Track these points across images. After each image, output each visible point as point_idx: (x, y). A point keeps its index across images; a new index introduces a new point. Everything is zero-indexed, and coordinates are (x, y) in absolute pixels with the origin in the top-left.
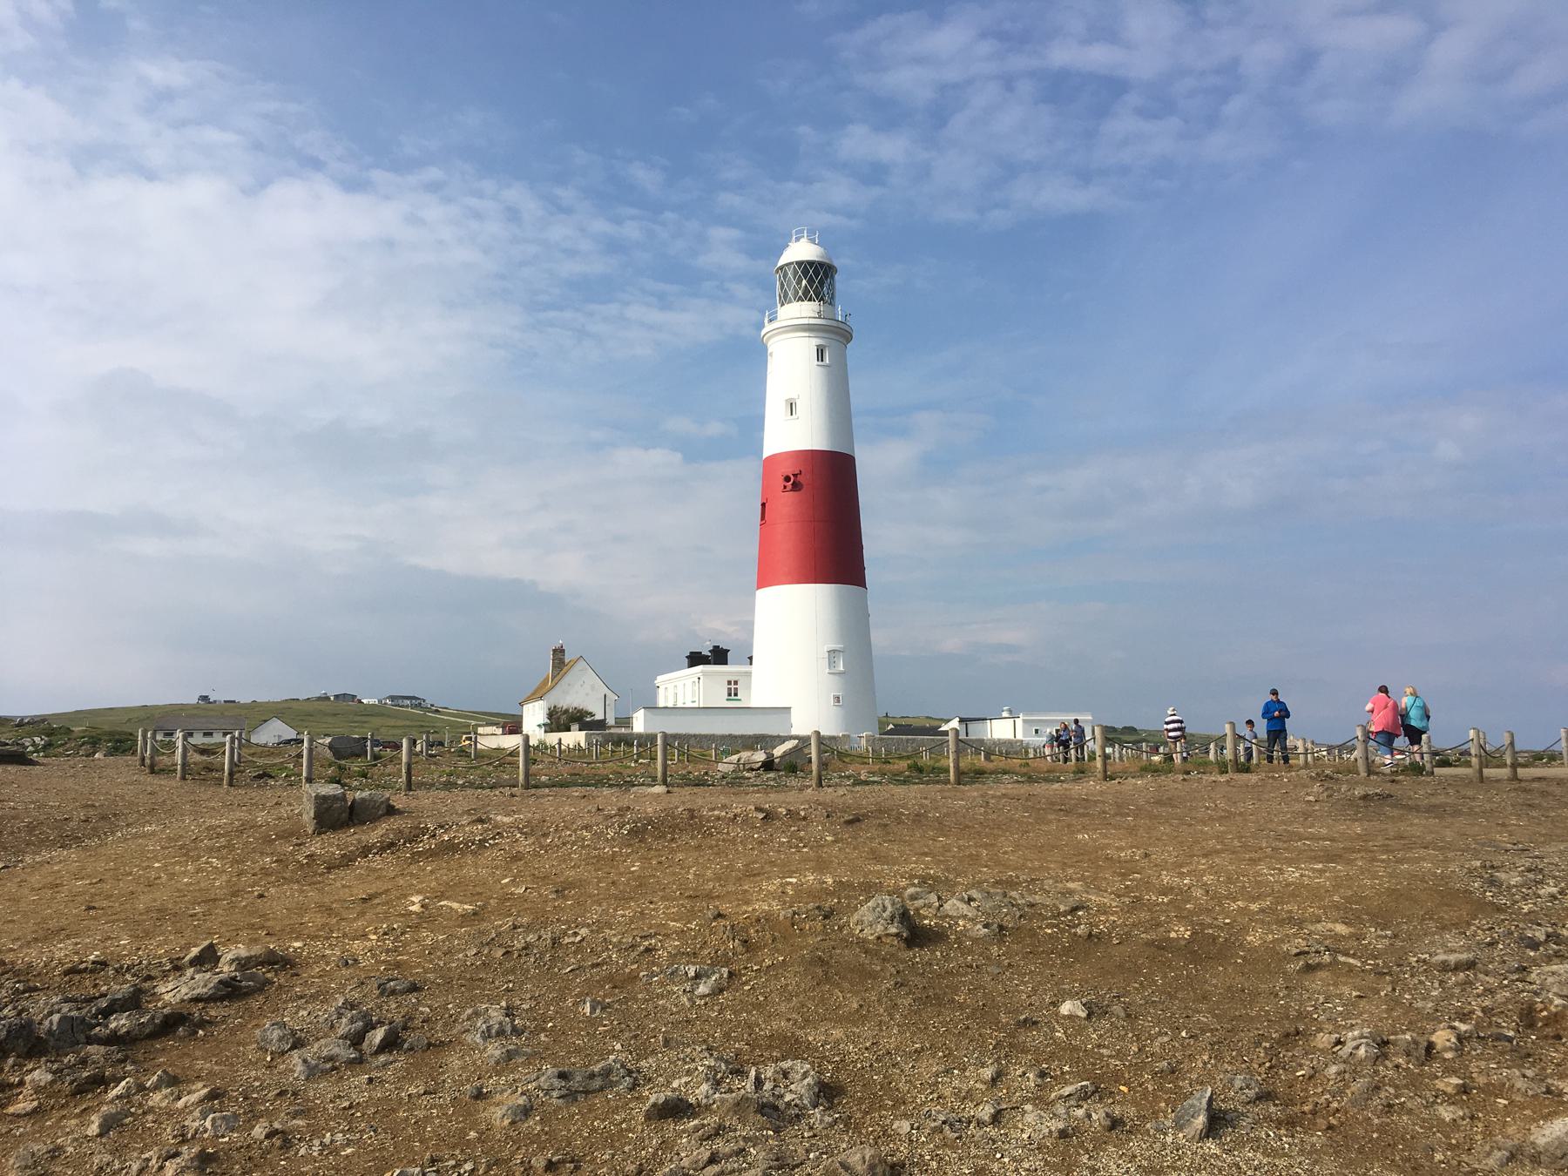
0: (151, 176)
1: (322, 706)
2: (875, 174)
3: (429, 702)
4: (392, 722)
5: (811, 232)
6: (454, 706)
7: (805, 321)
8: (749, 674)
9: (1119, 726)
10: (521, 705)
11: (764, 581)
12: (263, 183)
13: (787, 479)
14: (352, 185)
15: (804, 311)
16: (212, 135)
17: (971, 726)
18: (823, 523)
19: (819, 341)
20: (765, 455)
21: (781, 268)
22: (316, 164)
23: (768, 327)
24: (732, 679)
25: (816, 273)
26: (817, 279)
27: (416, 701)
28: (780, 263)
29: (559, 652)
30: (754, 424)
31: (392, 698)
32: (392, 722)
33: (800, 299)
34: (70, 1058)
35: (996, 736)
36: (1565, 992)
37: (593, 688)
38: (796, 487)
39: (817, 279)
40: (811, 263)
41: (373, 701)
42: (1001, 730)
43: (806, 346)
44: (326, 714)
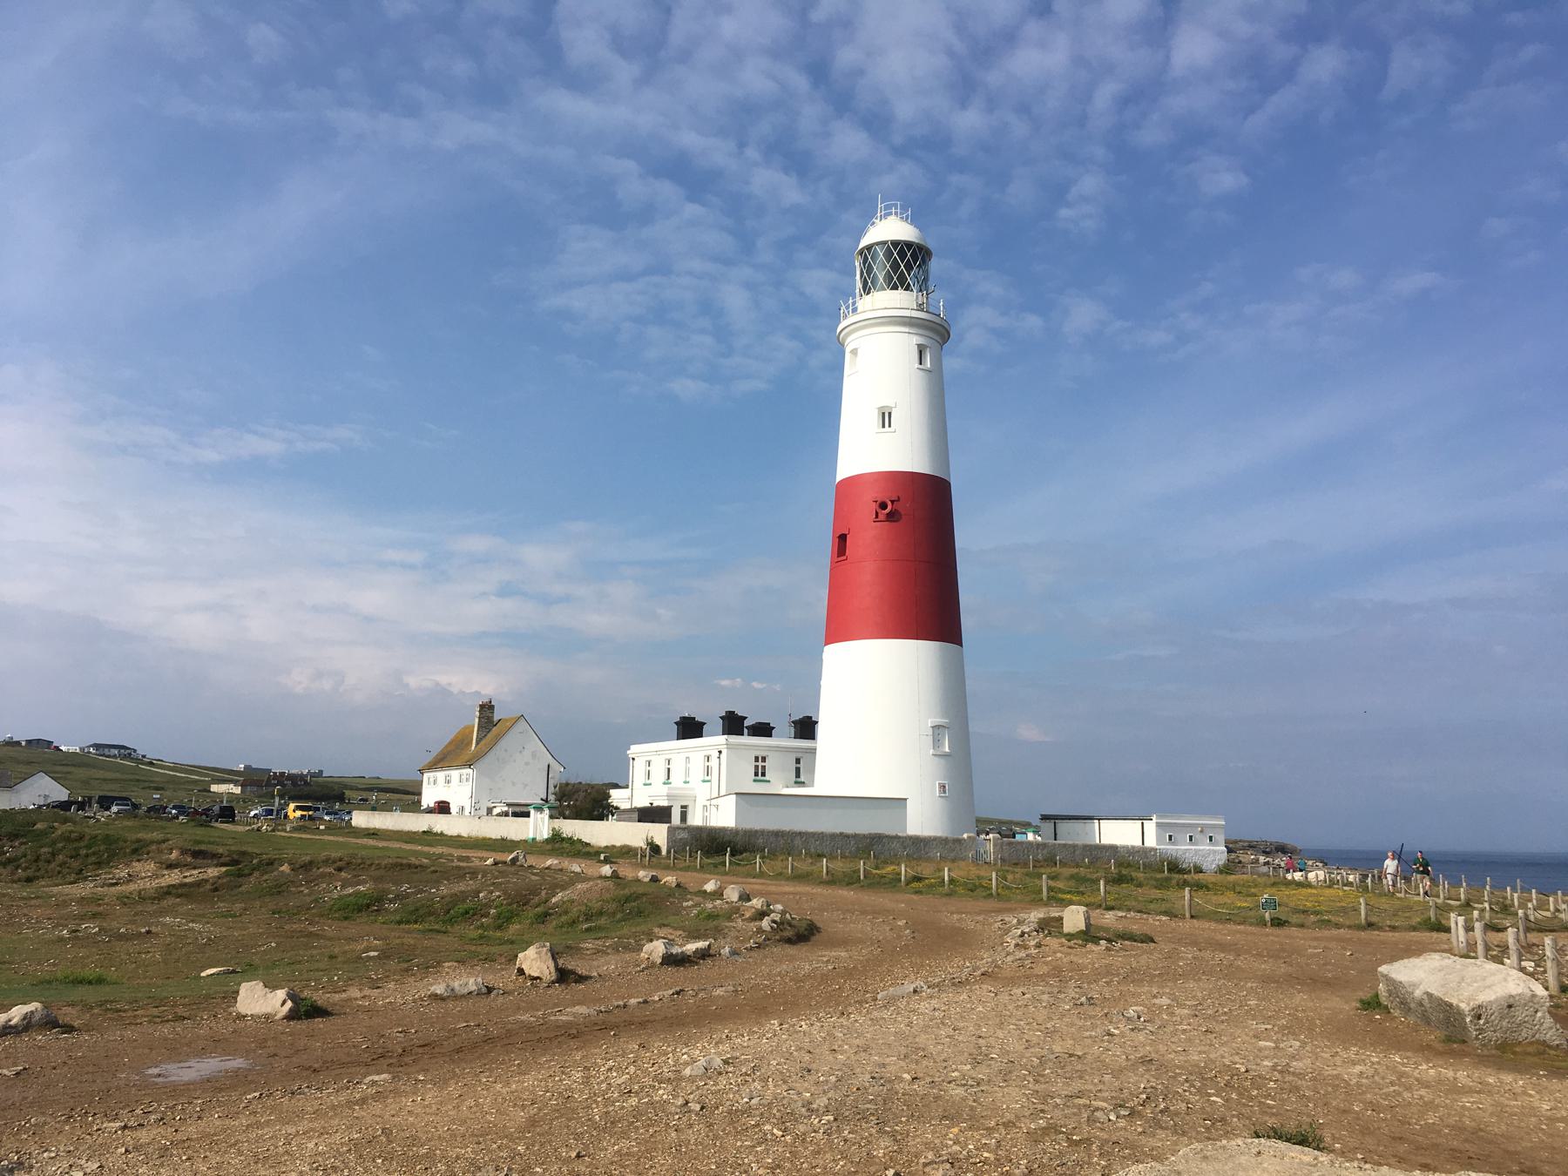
1: (11, 751)
3: (141, 752)
4: (101, 774)
5: (905, 209)
6: (169, 758)
7: (907, 313)
8: (813, 751)
10: (421, 771)
11: (838, 630)
13: (883, 506)
17: (1063, 827)
18: (912, 562)
19: (921, 340)
24: (760, 754)
25: (902, 254)
27: (126, 752)
28: (864, 243)
29: (487, 708)
31: (97, 746)
32: (101, 774)
33: (895, 288)
35: (1106, 841)
37: (534, 755)
38: (892, 517)
39: (907, 263)
41: (75, 749)
42: (1118, 833)
43: (905, 343)
44: (19, 762)
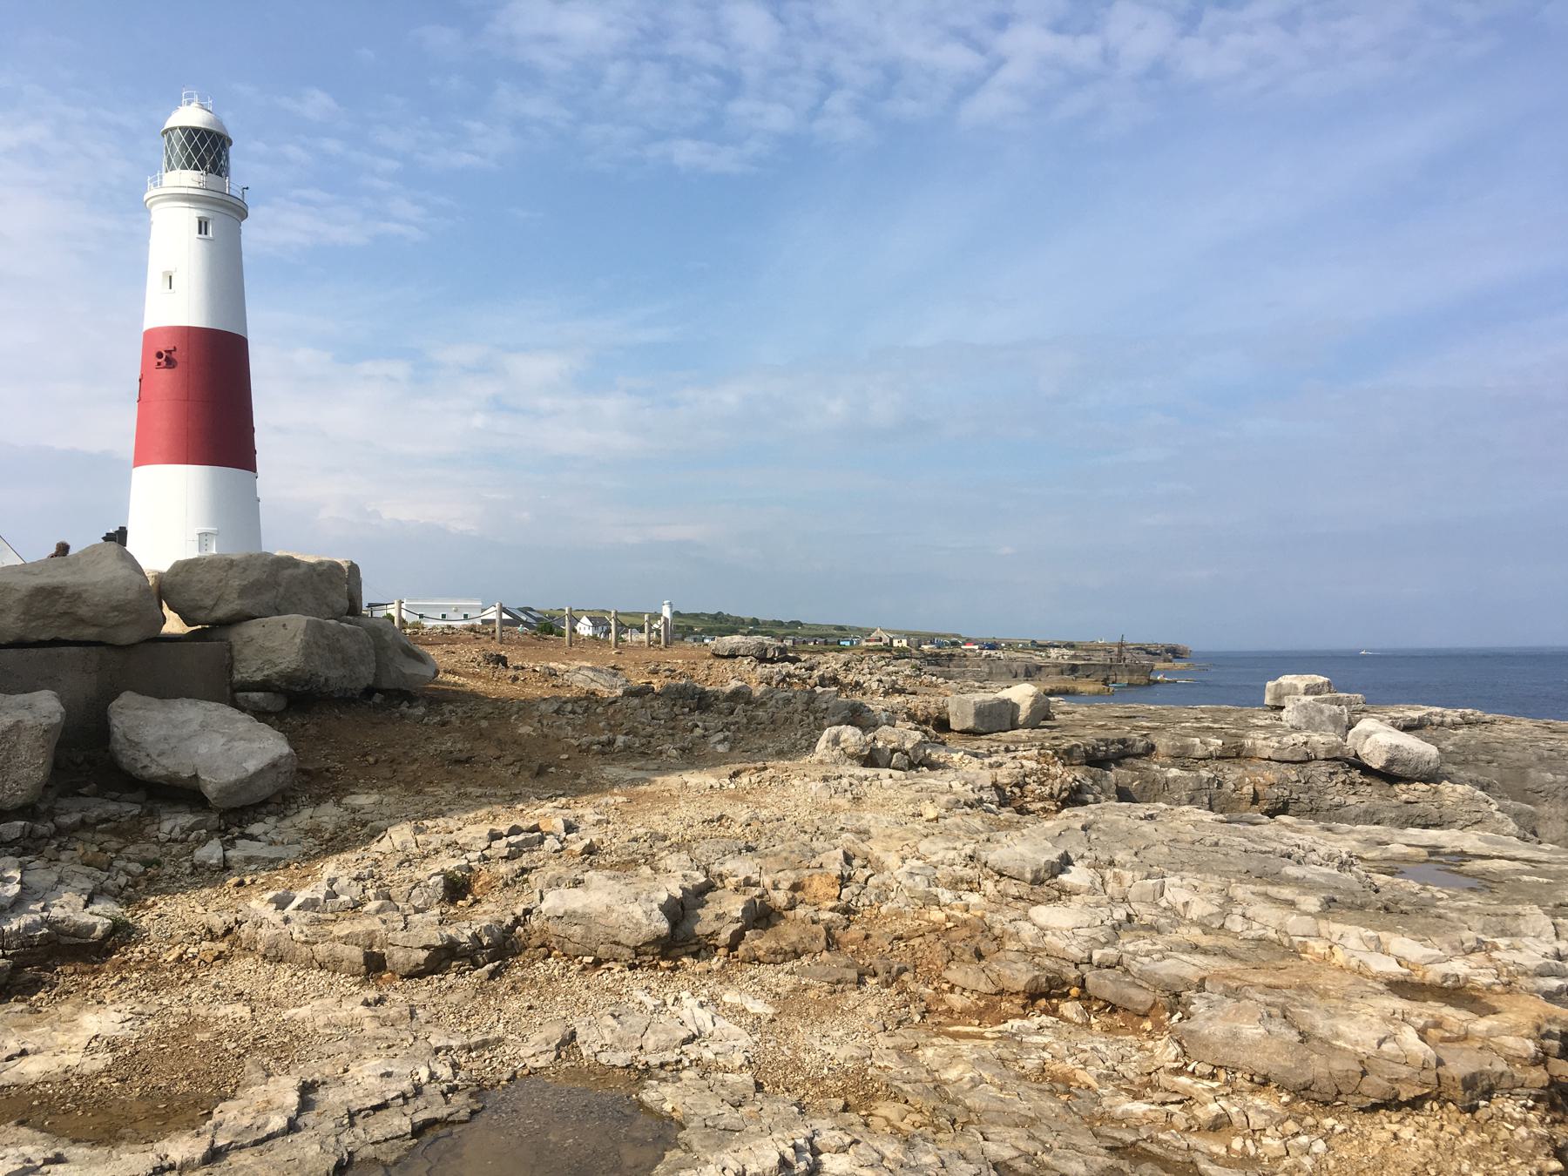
5: (202, 98)
7: (192, 191)
9: (786, 620)
11: (141, 458)
15: (188, 179)
20: (147, 326)
21: (166, 132)
23: (152, 192)
25: (202, 140)
26: (207, 149)
28: (168, 125)
33: (184, 168)
34: (472, 815)
36: (297, 975)
38: (170, 363)
39: (207, 149)
40: (196, 130)
43: (188, 216)
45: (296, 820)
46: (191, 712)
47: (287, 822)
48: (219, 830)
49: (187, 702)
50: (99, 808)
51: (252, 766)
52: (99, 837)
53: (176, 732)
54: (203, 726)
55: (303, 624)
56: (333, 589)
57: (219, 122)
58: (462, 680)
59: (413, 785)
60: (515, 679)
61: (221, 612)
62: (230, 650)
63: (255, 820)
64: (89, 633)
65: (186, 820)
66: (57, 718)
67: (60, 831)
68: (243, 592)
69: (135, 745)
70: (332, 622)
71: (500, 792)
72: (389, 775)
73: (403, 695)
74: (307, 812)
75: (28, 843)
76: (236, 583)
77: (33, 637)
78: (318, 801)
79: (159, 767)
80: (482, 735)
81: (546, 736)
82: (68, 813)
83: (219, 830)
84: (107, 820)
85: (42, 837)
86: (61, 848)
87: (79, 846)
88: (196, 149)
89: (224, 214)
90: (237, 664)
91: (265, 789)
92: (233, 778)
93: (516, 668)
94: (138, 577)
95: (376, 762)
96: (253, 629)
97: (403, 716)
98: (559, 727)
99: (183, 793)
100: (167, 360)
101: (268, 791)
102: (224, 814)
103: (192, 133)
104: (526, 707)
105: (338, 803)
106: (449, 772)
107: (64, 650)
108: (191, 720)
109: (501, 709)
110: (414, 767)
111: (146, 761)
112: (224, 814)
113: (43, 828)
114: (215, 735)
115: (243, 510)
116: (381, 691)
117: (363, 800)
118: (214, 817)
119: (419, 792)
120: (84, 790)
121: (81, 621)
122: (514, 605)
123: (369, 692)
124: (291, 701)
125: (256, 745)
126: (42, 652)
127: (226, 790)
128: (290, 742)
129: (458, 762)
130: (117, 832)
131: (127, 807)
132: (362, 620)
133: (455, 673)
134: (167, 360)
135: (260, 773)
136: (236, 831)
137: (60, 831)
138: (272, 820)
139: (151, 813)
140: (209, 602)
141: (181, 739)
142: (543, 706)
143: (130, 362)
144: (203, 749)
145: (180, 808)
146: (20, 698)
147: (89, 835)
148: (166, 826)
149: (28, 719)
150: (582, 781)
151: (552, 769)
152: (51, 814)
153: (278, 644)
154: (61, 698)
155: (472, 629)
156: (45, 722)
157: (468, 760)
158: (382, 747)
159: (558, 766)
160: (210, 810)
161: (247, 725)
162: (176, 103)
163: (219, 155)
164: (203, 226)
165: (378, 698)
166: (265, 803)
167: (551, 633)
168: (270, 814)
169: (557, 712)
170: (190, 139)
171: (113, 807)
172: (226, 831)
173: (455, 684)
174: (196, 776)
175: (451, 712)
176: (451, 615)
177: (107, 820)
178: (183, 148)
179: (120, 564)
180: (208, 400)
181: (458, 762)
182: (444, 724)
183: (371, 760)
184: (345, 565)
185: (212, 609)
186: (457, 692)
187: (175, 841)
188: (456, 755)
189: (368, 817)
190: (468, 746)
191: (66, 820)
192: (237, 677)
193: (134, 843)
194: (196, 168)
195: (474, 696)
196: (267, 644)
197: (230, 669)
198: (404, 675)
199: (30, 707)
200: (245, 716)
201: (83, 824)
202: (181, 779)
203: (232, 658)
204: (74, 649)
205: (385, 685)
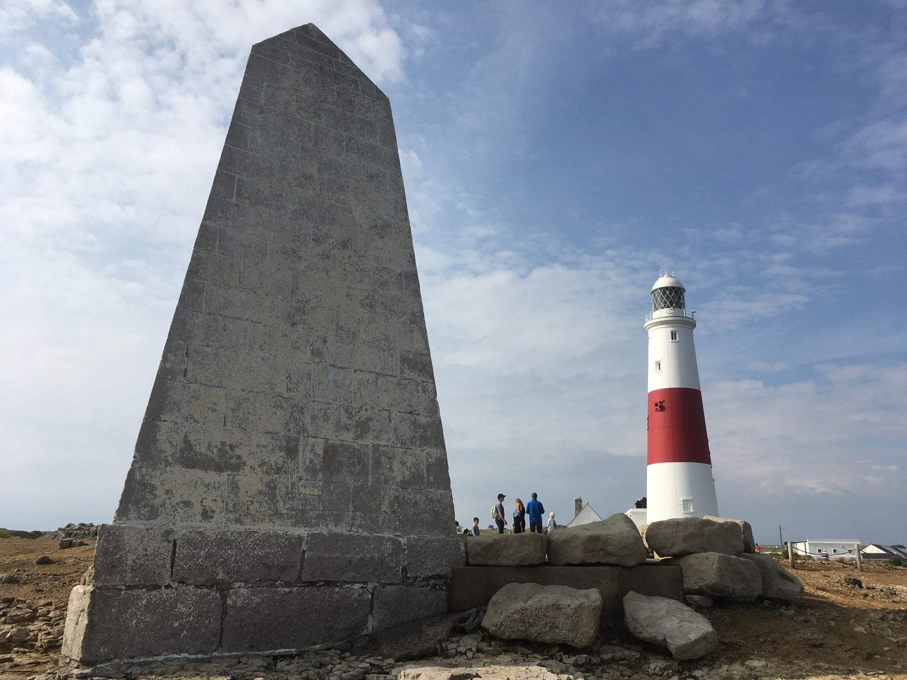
0: (476, 275)
2: (874, 210)
11: (651, 460)
12: (530, 270)
14: (574, 265)
15: (663, 313)
16: (506, 254)
18: (683, 426)
20: (649, 390)
22: (555, 259)
26: (674, 296)
29: (578, 502)
30: (643, 379)
38: (662, 408)
39: (674, 296)
40: (667, 288)
42: (801, 549)
45: (720, 671)
46: (662, 605)
47: (714, 672)
48: (678, 671)
49: (660, 598)
50: (621, 652)
51: (693, 637)
52: (621, 668)
53: (654, 615)
54: (668, 612)
55: (717, 558)
56: (737, 539)
57: (678, 282)
58: (828, 595)
59: (786, 658)
60: (866, 596)
61: (675, 550)
62: (681, 571)
63: (697, 668)
64: (613, 560)
65: (662, 664)
66: (598, 603)
67: (603, 662)
68: (686, 539)
69: (635, 620)
70: (734, 557)
71: (840, 668)
72: (772, 650)
73: (784, 602)
74: (725, 667)
75: (589, 667)
76: (681, 534)
77: (588, 561)
78: (731, 661)
79: (647, 633)
80: (830, 630)
81: (874, 634)
82: (606, 653)
83: (678, 671)
84: (624, 659)
85: (595, 664)
86: (603, 671)
87: (610, 671)
88: (668, 298)
89: (683, 328)
90: (685, 579)
91: (701, 651)
92: (683, 642)
93: (868, 588)
94: (633, 532)
95: (765, 641)
96: (691, 560)
97: (781, 615)
98: (882, 629)
99: (658, 648)
100: (661, 407)
101: (702, 653)
102: (682, 662)
103: (664, 290)
104: (860, 614)
105: (743, 664)
106: (809, 652)
107: (601, 568)
108: (661, 609)
109: (845, 614)
110: (787, 647)
111: (641, 629)
112: (682, 662)
113: (595, 660)
114: (674, 618)
115: (702, 490)
116: (769, 599)
117: (757, 664)
118: (676, 664)
119: (789, 663)
120: (614, 642)
121: (609, 554)
122: (888, 543)
123: (761, 599)
124: (714, 602)
125: (695, 625)
126: (592, 569)
127: (681, 649)
128: (713, 625)
129: (814, 646)
130: (629, 666)
131: (633, 653)
132: (754, 556)
133: (823, 589)
134: (661, 407)
135: (697, 641)
136: (687, 673)
137: (603, 662)
138: (706, 669)
139: (645, 658)
140: (669, 545)
141: (657, 619)
142: (872, 615)
143: (643, 410)
144: (668, 625)
145: (659, 657)
146: (583, 591)
147: (616, 666)
148: (652, 666)
149: (586, 602)
150: (899, 666)
151: (877, 656)
152: (599, 653)
153: (706, 567)
154: (601, 593)
155: (841, 561)
156: (593, 604)
157: (821, 645)
158: (769, 632)
159: (882, 655)
160: (674, 660)
161: (690, 613)
162: (656, 279)
163: (679, 298)
164: (673, 336)
165: (766, 603)
166: (702, 659)
167: (900, 564)
168: (705, 665)
169: (882, 619)
170: (664, 293)
171: (627, 652)
172: (682, 673)
173: (823, 597)
174: (665, 640)
175: (812, 614)
176: (840, 550)
177: (624, 659)
178: (662, 298)
179: (625, 525)
180: (683, 426)
181: (814, 646)
182: (806, 622)
183: (761, 640)
184: (741, 524)
185: (671, 548)
186: (821, 602)
187: (657, 675)
188: (813, 642)
189: (758, 674)
190: (821, 636)
191: (606, 657)
192: (685, 586)
193: (637, 673)
194: (668, 307)
195: (833, 605)
196: (699, 568)
197: (682, 581)
198: (781, 590)
199: (587, 596)
200: (689, 608)
201: (613, 660)
202: (657, 641)
203: (682, 575)
204: (607, 568)
205: (771, 596)
